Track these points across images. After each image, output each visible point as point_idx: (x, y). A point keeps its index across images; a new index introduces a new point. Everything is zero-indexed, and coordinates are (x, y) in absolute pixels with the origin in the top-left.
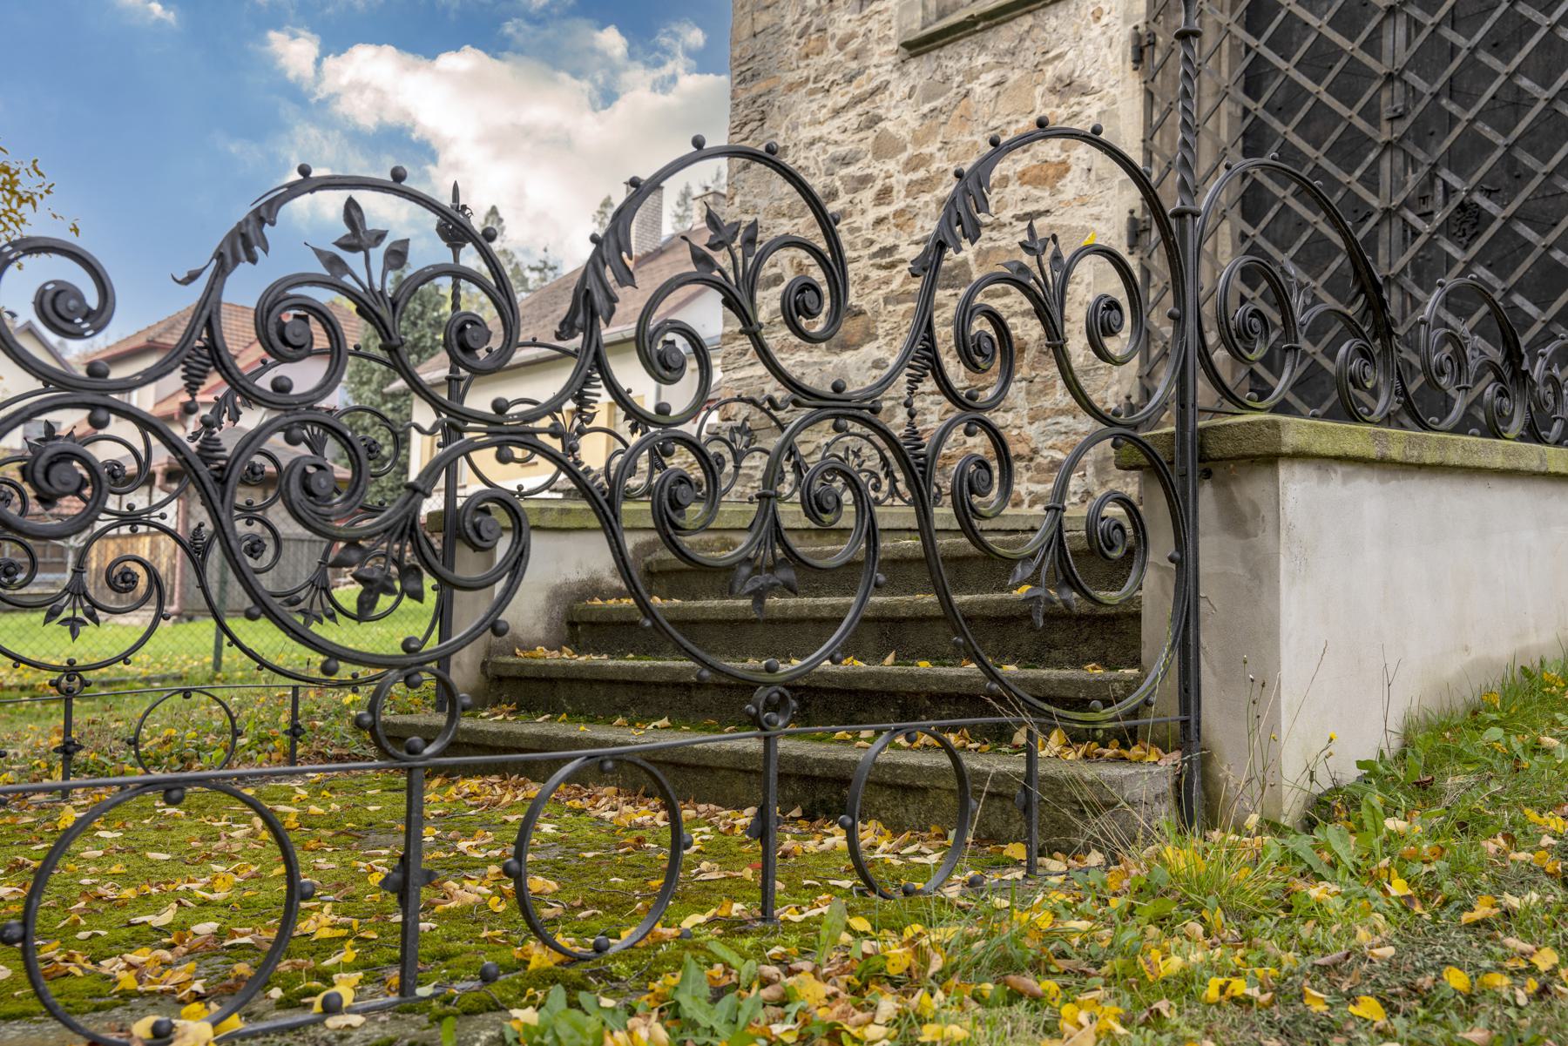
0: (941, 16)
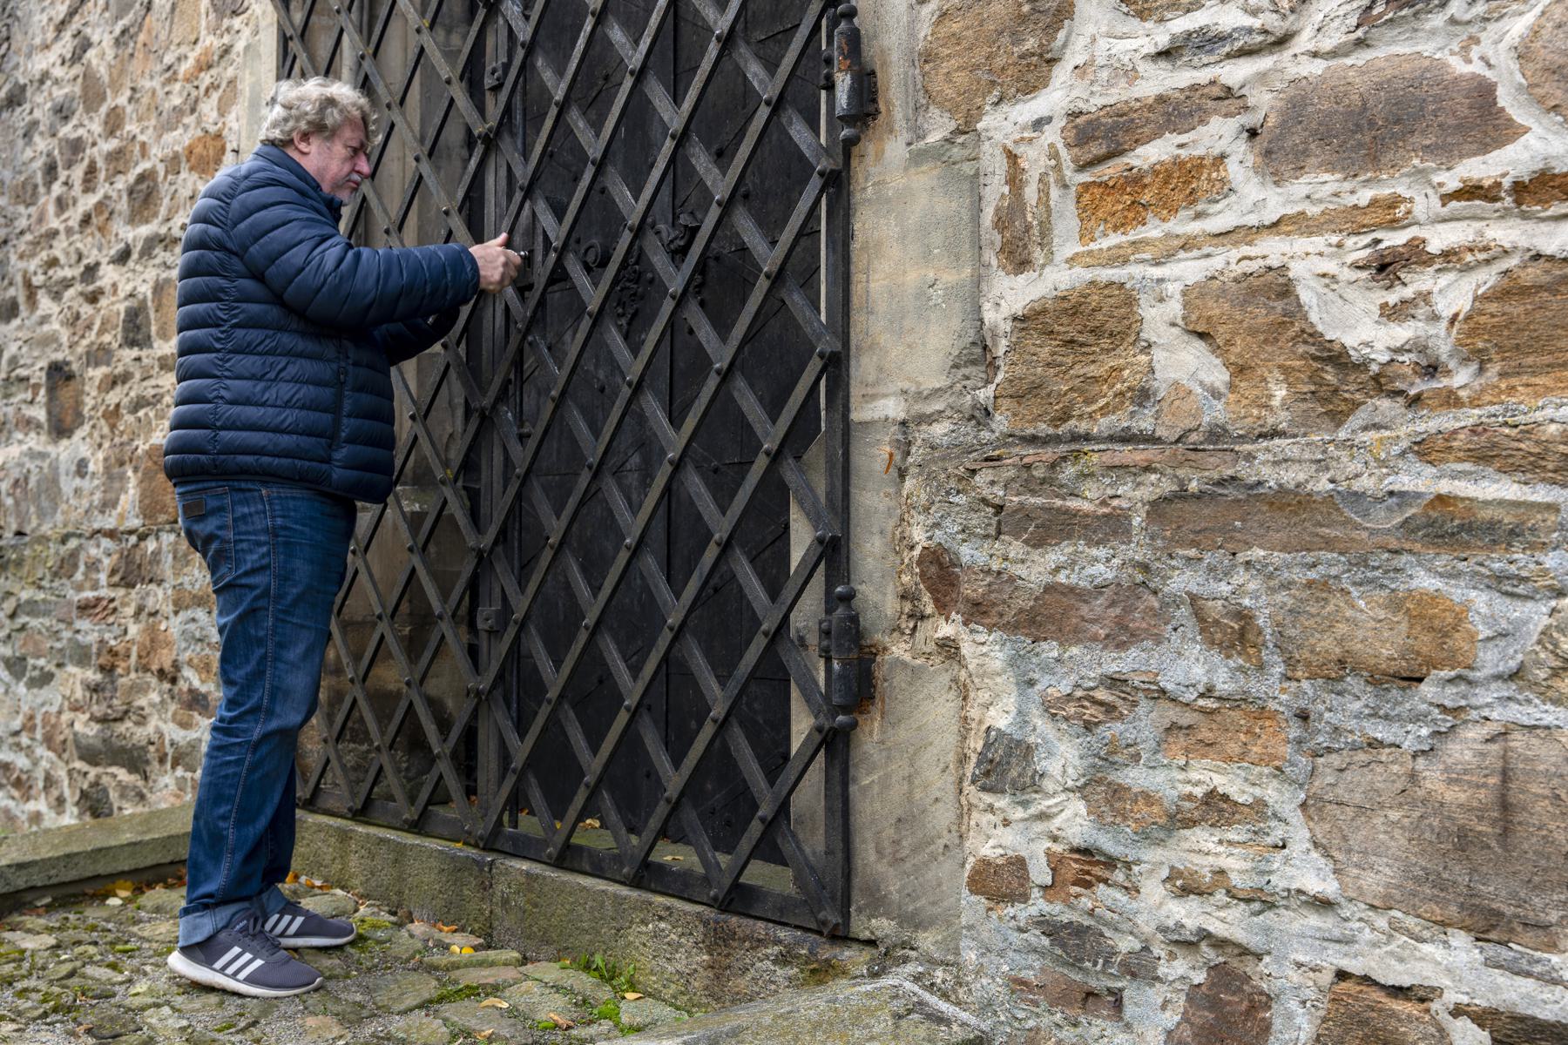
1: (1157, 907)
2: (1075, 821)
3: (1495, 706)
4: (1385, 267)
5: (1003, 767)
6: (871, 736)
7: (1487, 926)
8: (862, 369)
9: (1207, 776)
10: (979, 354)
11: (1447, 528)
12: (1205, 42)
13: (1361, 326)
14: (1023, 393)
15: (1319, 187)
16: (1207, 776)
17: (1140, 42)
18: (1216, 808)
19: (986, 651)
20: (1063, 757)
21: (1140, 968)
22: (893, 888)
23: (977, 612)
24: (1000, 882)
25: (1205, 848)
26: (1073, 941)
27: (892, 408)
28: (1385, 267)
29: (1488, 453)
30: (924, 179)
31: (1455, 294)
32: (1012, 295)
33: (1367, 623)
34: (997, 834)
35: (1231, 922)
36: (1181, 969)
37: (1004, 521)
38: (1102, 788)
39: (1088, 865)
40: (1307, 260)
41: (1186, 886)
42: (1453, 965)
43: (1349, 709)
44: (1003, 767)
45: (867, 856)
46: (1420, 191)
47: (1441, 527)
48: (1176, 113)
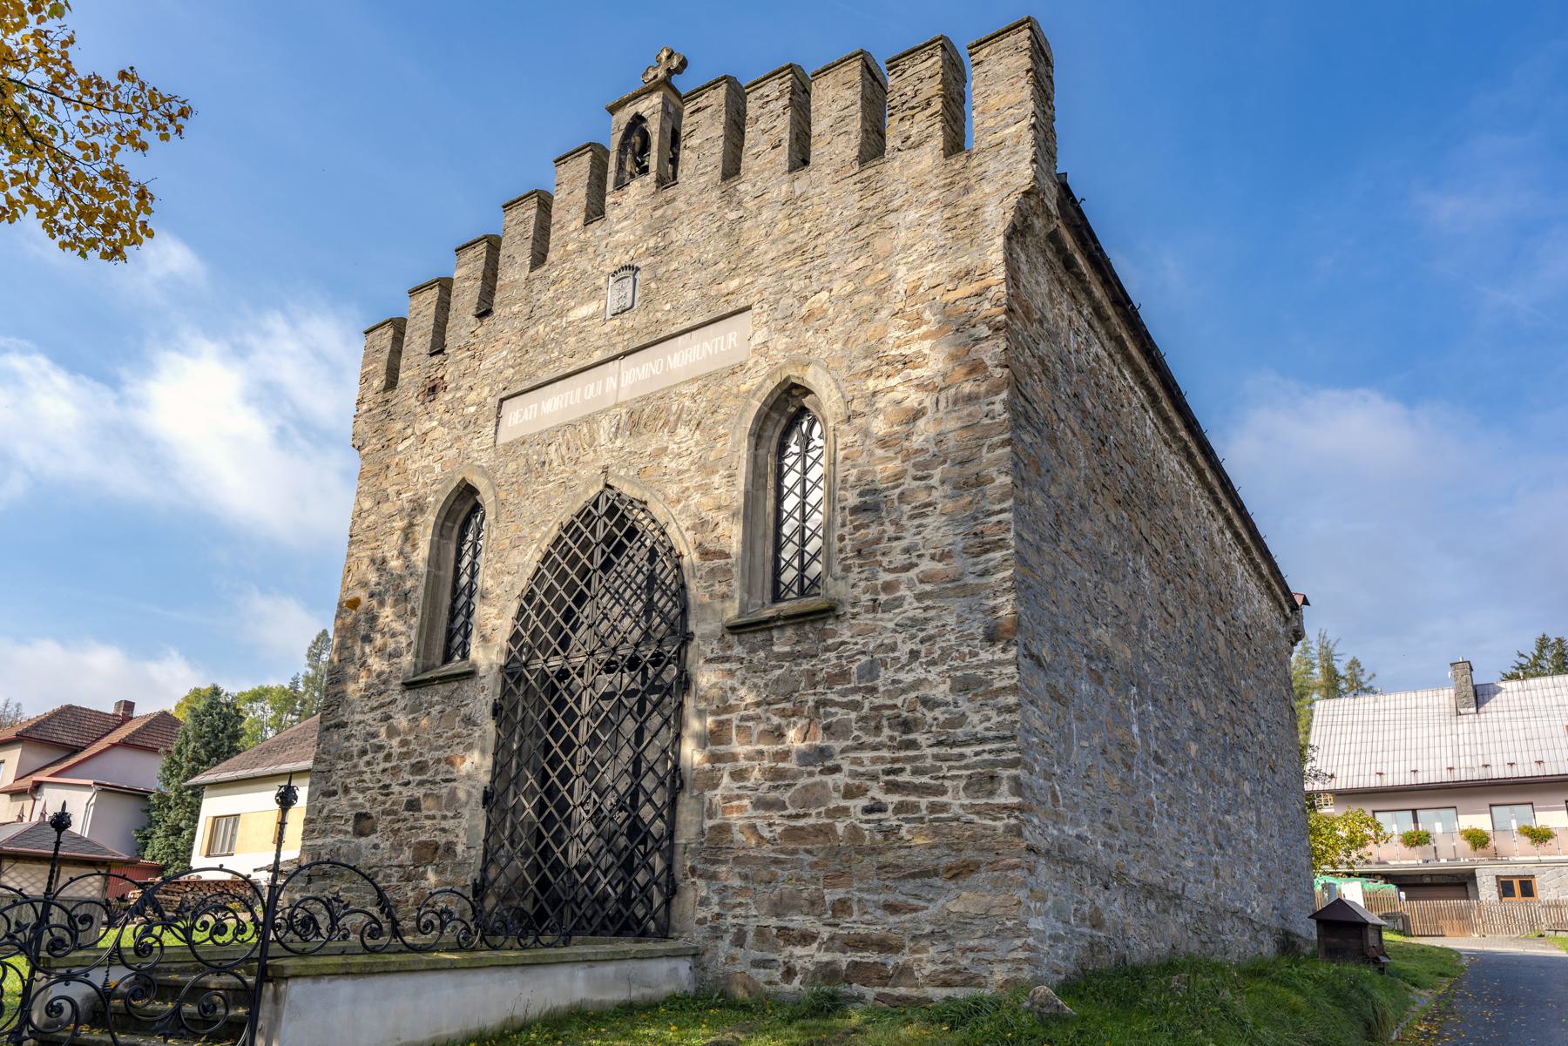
0: (425, 670)
1: (730, 920)
2: (716, 909)
3: (780, 885)
4: (770, 825)
5: (704, 902)
6: (675, 901)
7: (778, 915)
8: (678, 833)
9: (740, 900)
10: (702, 833)
11: (776, 862)
12: (745, 787)
13: (766, 834)
14: (709, 840)
15: (761, 812)
16: (740, 900)
17: (673, 465)
18: (740, 904)
19: (701, 883)
20: (715, 899)
21: (726, 931)
22: (678, 926)
23: (700, 876)
24: (701, 922)
25: (738, 911)
26: (714, 929)
27: (683, 841)
28: (770, 825)
29: (782, 852)
30: (693, 801)
31: (779, 830)
32: (708, 823)
33: (764, 874)
34: (701, 913)
35: (741, 921)
36: (734, 930)
37: (706, 861)
38: (721, 904)
39: (719, 916)
40: (759, 822)
41: (735, 917)
42: (773, 922)
43: (761, 888)
44: (704, 902)
45: (673, 922)
46: (775, 816)
47: (1069, 524)
48: (739, 797)
